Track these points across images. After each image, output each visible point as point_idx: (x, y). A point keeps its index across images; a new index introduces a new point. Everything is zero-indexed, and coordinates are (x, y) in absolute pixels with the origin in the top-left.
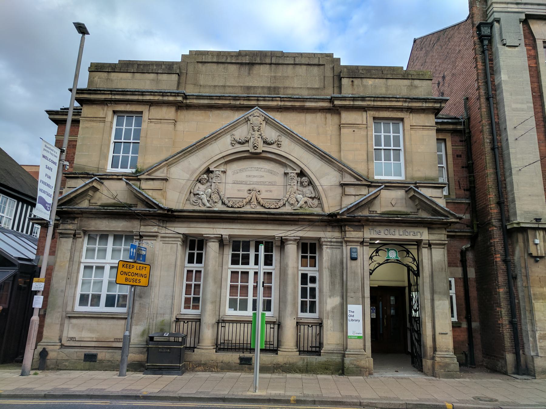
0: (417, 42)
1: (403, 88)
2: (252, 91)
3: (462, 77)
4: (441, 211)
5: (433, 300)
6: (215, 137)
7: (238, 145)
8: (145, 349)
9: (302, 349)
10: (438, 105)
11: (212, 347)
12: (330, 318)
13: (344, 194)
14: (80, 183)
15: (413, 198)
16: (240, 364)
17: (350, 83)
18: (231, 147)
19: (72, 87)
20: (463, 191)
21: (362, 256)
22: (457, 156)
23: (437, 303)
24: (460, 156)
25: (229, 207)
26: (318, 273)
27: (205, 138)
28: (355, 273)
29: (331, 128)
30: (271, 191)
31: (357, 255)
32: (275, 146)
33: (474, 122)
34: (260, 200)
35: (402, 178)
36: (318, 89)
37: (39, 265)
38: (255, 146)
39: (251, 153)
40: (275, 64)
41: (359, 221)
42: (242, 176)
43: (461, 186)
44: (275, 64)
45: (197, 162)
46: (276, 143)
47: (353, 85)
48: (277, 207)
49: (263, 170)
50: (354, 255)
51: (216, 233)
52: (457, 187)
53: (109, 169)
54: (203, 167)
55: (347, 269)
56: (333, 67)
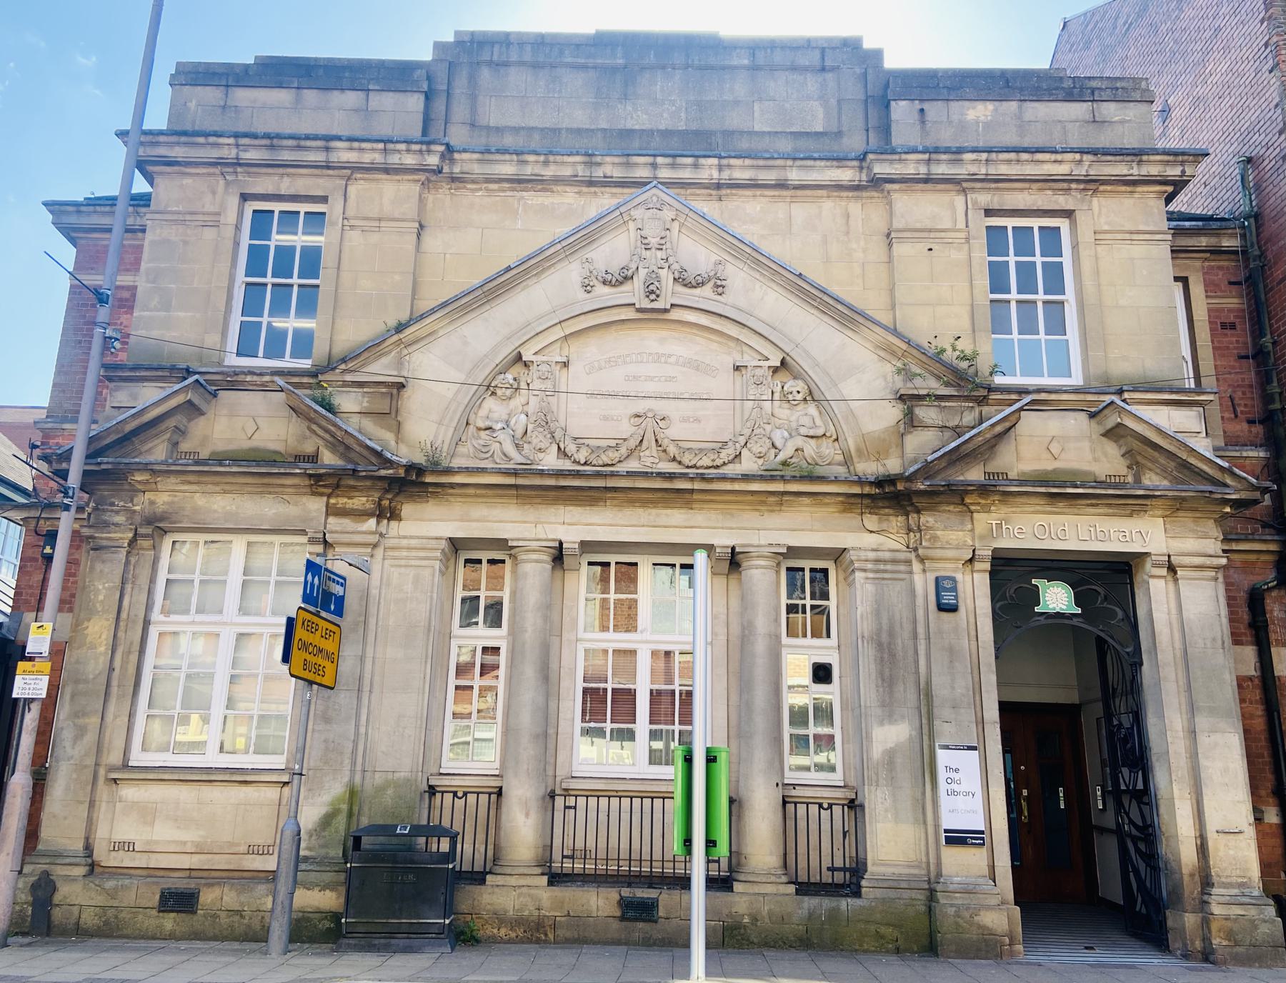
0: (1071, 27)
1: (1069, 126)
2: (636, 144)
3: (1227, 102)
4: (1205, 468)
5: (1192, 733)
6: (533, 266)
7: (601, 290)
8: (342, 876)
9: (803, 877)
10: (1174, 172)
11: (539, 870)
12: (882, 781)
13: (910, 422)
14: (149, 395)
15: (1115, 433)
16: (623, 918)
17: (916, 116)
18: (581, 294)
19: (127, 126)
20: (1245, 426)
21: (970, 601)
22: (1222, 326)
23: (1204, 740)
24: (1233, 326)
25: (579, 463)
26: (836, 655)
27: (509, 269)
28: (952, 652)
29: (862, 243)
30: (697, 420)
31: (956, 597)
32: (707, 290)
33: (1275, 226)
34: (665, 442)
35: (1077, 379)
36: (818, 134)
37: (20, 638)
38: (652, 292)
39: (640, 310)
40: (700, 68)
41: (743, 628)
42: (614, 379)
43: (1238, 410)
44: (700, 68)
45: (483, 336)
46: (711, 284)
47: (923, 122)
48: (719, 462)
49: (672, 360)
50: (948, 599)
51: (543, 536)
52: (1227, 415)
53: (233, 361)
54: (507, 351)
55: (928, 638)
56: (865, 74)
